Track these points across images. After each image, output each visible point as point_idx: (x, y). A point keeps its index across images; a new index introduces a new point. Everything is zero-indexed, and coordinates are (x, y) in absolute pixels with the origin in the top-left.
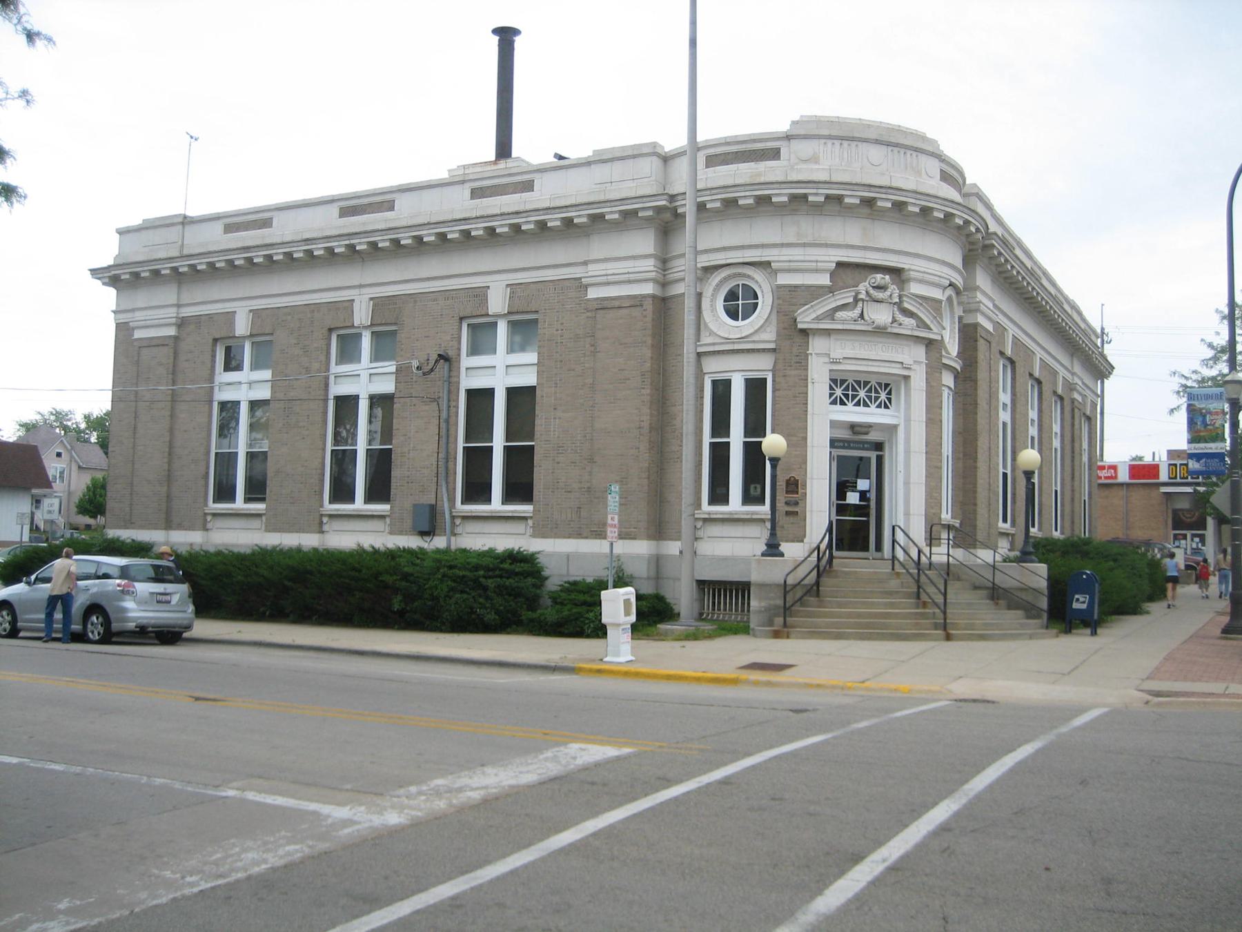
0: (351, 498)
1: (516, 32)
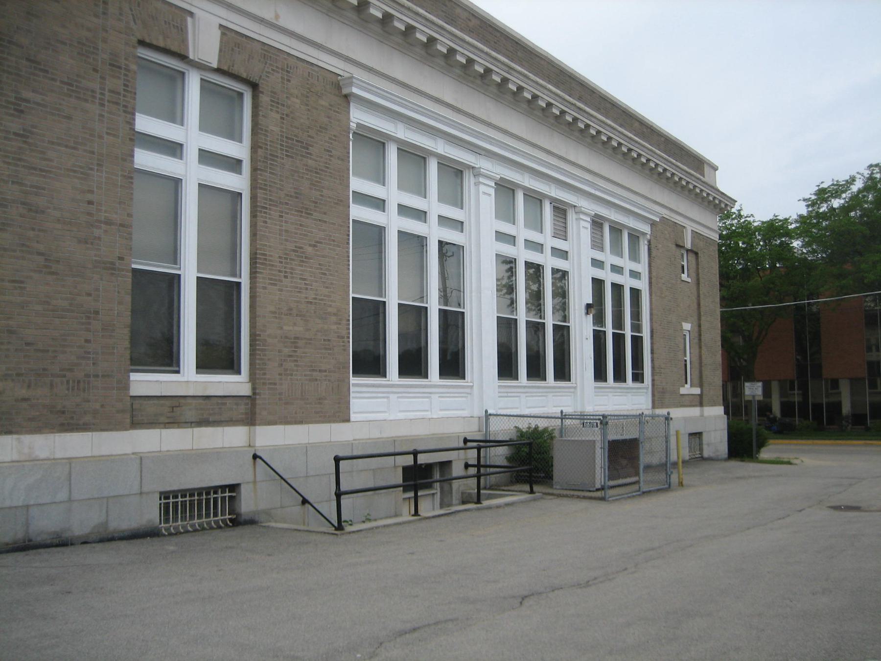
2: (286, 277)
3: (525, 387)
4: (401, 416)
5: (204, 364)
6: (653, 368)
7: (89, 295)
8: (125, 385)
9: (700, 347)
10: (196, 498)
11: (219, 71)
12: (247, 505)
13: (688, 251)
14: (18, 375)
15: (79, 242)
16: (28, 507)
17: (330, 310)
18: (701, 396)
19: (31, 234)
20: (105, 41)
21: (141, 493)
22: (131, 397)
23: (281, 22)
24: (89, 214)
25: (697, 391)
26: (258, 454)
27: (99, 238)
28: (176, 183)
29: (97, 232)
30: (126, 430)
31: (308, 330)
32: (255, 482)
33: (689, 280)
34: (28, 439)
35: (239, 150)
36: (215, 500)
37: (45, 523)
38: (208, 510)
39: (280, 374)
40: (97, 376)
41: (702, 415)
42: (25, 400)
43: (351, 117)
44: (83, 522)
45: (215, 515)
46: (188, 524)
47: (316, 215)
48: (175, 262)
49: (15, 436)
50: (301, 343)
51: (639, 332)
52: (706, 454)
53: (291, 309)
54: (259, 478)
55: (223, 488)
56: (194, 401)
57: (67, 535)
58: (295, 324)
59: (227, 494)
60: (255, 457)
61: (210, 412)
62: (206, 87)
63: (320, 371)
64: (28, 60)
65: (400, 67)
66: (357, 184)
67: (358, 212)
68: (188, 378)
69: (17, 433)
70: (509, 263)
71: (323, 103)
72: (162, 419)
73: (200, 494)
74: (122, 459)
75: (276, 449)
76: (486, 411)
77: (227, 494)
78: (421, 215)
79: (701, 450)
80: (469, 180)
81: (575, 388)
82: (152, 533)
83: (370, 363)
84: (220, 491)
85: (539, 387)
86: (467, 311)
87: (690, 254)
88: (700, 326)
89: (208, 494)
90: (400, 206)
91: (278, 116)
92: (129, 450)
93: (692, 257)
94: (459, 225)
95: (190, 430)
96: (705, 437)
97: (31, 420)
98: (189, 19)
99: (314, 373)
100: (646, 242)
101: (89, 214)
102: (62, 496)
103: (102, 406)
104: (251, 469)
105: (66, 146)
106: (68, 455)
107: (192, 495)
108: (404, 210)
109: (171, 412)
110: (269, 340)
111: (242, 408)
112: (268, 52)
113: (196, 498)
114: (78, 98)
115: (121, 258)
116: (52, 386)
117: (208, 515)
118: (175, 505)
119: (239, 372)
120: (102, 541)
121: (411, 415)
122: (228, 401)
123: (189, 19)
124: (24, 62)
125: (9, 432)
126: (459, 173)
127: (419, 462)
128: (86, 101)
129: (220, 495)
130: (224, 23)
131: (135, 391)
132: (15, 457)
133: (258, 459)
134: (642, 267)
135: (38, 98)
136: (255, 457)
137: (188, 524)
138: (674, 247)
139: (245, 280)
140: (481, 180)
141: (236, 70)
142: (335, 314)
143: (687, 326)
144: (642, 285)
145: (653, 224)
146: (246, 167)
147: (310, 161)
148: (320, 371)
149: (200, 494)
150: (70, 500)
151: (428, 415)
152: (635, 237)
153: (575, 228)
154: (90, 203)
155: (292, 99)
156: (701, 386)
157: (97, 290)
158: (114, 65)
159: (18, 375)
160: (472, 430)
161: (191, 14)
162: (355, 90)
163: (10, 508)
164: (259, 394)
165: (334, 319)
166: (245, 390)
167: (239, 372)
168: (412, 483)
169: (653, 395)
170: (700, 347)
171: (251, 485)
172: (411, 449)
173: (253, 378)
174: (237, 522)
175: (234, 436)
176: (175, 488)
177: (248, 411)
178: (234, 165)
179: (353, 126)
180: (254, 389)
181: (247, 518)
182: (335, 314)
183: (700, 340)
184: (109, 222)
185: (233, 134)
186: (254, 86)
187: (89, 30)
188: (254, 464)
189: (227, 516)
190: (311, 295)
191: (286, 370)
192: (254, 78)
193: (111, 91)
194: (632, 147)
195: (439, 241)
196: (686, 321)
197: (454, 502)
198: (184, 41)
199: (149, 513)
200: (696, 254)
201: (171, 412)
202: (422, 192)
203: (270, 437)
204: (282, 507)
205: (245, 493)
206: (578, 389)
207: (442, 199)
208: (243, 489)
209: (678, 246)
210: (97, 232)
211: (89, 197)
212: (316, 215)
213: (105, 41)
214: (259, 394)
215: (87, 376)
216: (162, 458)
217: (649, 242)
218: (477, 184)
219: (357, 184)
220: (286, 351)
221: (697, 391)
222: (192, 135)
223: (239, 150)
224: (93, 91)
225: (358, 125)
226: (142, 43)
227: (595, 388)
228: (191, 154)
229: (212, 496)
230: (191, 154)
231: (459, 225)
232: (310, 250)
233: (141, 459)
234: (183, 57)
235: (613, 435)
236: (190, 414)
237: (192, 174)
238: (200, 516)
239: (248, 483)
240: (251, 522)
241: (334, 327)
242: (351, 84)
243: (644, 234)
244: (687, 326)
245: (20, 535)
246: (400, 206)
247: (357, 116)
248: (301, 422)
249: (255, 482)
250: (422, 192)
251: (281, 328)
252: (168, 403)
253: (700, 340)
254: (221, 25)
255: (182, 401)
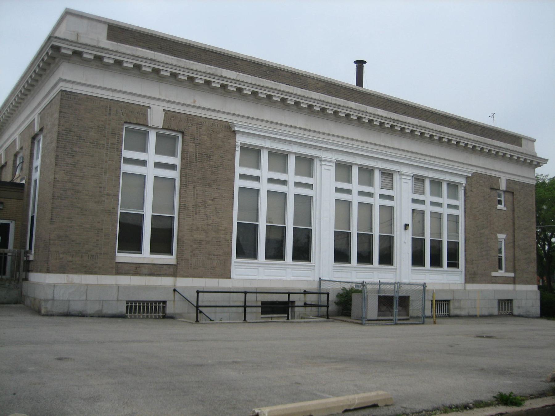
0: (138, 248)
1: (365, 62)
2: (196, 214)
3: (355, 267)
4: (265, 278)
5: (153, 250)
6: (466, 260)
7: (99, 223)
8: (114, 257)
9: (514, 249)
11: (163, 128)
12: (169, 310)
13: (504, 191)
14: (69, 252)
15: (95, 203)
16: (69, 301)
17: (220, 228)
18: (514, 278)
19: (75, 200)
20: (109, 124)
22: (116, 263)
23: (197, 104)
24: (100, 192)
25: (512, 275)
26: (177, 289)
27: (104, 201)
28: (371, 205)
29: (103, 199)
30: (113, 275)
31: (207, 237)
33: (505, 209)
34: (71, 276)
35: (176, 161)
36: (155, 307)
37: (76, 307)
38: (151, 310)
39: (191, 256)
40: (101, 254)
41: (465, 289)
42: (71, 261)
43: (237, 141)
44: (92, 308)
47: (214, 186)
48: (143, 209)
49: (66, 275)
50: (203, 243)
51: (391, 233)
53: (198, 228)
54: (176, 299)
55: (160, 302)
56: (147, 266)
57: (84, 313)
58: (200, 234)
60: (175, 290)
61: (155, 270)
62: (158, 136)
63: (214, 255)
64: (77, 136)
65: (268, 114)
66: (239, 170)
67: (126, 168)
68: (146, 255)
69: (67, 273)
70: (439, 216)
71: (221, 136)
72: (131, 272)
74: (110, 286)
75: (186, 288)
76: (320, 278)
78: (440, 205)
79: (512, 310)
80: (396, 177)
81: (396, 269)
82: (122, 316)
83: (247, 250)
85: (248, 263)
86: (395, 235)
87: (507, 195)
88: (514, 236)
90: (295, 183)
91: (194, 145)
92: (114, 283)
93: (509, 196)
94: (391, 198)
95: (145, 277)
96: (515, 304)
97: (73, 269)
98: (149, 110)
99: (211, 256)
100: (463, 188)
101: (100, 192)
102: (84, 298)
103: (103, 265)
105: (92, 167)
106: (87, 283)
108: (449, 206)
109: (136, 269)
110: (186, 241)
111: (172, 270)
112: (189, 118)
114: (97, 148)
115: (113, 208)
116: (82, 257)
117: (147, 312)
118: (135, 307)
119: (172, 255)
120: (99, 317)
121: (272, 278)
122: (164, 267)
123: (149, 110)
124: (76, 138)
125: (64, 273)
126: (391, 175)
127: (290, 300)
128: (100, 149)
130: (166, 109)
131: (118, 260)
132: (66, 282)
133: (176, 292)
134: (460, 202)
135: (80, 150)
136: (175, 290)
138: (488, 190)
139: (176, 215)
140: (403, 177)
141: (172, 127)
142: (224, 230)
143: (502, 237)
144: (460, 213)
145: (467, 178)
146: (179, 168)
147: (211, 163)
148: (214, 255)
150: (86, 300)
151: (284, 278)
152: (453, 187)
153: (398, 183)
154: (100, 188)
155: (202, 136)
156: (514, 271)
157: (103, 221)
158: (113, 134)
159: (69, 252)
160: (313, 287)
161: (150, 108)
162: (236, 129)
163: (62, 300)
164: (180, 264)
165: (223, 232)
166: (174, 262)
167: (172, 255)
168: (290, 309)
169: (466, 275)
170: (514, 249)
171: (172, 302)
172: (287, 291)
173: (179, 257)
174: (164, 317)
175: (167, 281)
177: (173, 271)
178: (128, 161)
179: (238, 144)
180: (177, 262)
182: (224, 230)
183: (514, 244)
184: (108, 195)
185: (173, 154)
186: (183, 133)
187: (102, 121)
190: (210, 222)
191: (194, 254)
192: (183, 130)
193: (111, 144)
194: (498, 150)
195: (413, 210)
196: (501, 232)
198: (146, 119)
199: (122, 309)
200: (513, 193)
201: (136, 269)
202: (349, 181)
203: (183, 283)
204: (188, 313)
206: (398, 270)
207: (432, 194)
208: (168, 303)
209: (492, 189)
210: (103, 199)
211: (100, 185)
212: (214, 186)
213: (109, 124)
214: (180, 264)
215: (97, 253)
216: (128, 288)
217: (465, 188)
218: (321, 165)
219: (126, 154)
220: (195, 246)
221: (512, 275)
222: (151, 156)
223: (176, 161)
224: (104, 145)
225: (241, 143)
226: (126, 122)
227: (412, 270)
228: (445, 206)
230: (445, 206)
231: (391, 198)
232: (210, 202)
233: (118, 287)
234: (147, 126)
235: (401, 294)
236: (145, 271)
237: (150, 173)
239: (170, 301)
241: (223, 236)
242: (234, 126)
243: (461, 184)
244: (502, 237)
245: (66, 311)
246: (295, 183)
247: (240, 140)
248: (202, 277)
249: (174, 301)
250: (349, 181)
251: (192, 236)
252: (134, 265)
253: (514, 244)
254: (164, 110)
255: (141, 265)
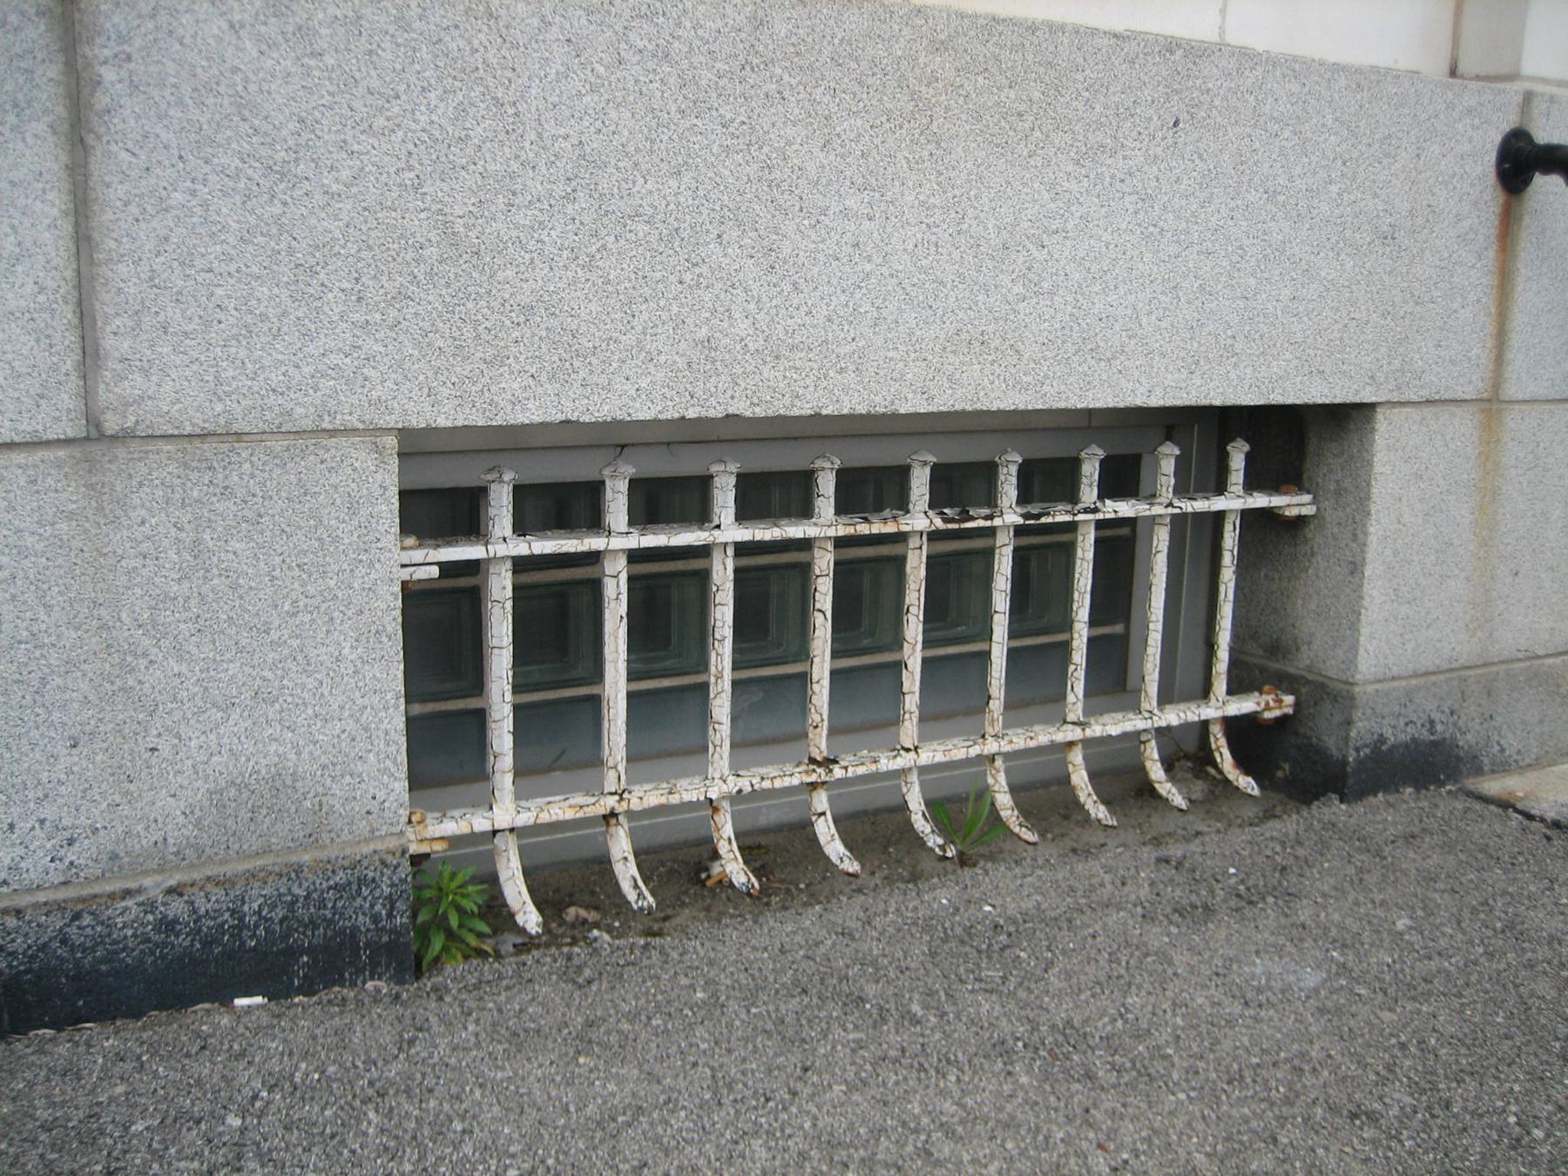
10: (919, 519)
12: (1404, 608)
21: (95, 437)
32: (1491, 404)
36: (1120, 548)
45: (1112, 676)
46: (815, 771)
52: (111, 424)
55: (1206, 432)
59: (1234, 501)
73: (961, 485)
77: (1234, 501)
84: (1167, 459)
89: (1048, 479)
104: (1477, 274)
107: (869, 489)
113: (919, 519)
117: (1037, 675)
129: (1161, 504)
137: (815, 771)
149: (961, 485)
171: (1462, 428)
174: (1294, 759)
176: (639, 389)
181: (1396, 733)
188: (1508, 223)
189: (1223, 705)
197: (1162, 539)
205: (1405, 490)
229: (1091, 508)
238: (955, 689)
240: (1428, 764)
